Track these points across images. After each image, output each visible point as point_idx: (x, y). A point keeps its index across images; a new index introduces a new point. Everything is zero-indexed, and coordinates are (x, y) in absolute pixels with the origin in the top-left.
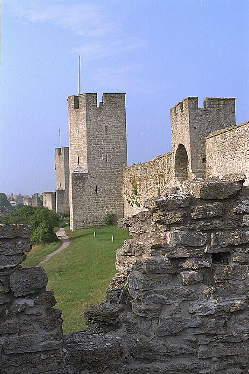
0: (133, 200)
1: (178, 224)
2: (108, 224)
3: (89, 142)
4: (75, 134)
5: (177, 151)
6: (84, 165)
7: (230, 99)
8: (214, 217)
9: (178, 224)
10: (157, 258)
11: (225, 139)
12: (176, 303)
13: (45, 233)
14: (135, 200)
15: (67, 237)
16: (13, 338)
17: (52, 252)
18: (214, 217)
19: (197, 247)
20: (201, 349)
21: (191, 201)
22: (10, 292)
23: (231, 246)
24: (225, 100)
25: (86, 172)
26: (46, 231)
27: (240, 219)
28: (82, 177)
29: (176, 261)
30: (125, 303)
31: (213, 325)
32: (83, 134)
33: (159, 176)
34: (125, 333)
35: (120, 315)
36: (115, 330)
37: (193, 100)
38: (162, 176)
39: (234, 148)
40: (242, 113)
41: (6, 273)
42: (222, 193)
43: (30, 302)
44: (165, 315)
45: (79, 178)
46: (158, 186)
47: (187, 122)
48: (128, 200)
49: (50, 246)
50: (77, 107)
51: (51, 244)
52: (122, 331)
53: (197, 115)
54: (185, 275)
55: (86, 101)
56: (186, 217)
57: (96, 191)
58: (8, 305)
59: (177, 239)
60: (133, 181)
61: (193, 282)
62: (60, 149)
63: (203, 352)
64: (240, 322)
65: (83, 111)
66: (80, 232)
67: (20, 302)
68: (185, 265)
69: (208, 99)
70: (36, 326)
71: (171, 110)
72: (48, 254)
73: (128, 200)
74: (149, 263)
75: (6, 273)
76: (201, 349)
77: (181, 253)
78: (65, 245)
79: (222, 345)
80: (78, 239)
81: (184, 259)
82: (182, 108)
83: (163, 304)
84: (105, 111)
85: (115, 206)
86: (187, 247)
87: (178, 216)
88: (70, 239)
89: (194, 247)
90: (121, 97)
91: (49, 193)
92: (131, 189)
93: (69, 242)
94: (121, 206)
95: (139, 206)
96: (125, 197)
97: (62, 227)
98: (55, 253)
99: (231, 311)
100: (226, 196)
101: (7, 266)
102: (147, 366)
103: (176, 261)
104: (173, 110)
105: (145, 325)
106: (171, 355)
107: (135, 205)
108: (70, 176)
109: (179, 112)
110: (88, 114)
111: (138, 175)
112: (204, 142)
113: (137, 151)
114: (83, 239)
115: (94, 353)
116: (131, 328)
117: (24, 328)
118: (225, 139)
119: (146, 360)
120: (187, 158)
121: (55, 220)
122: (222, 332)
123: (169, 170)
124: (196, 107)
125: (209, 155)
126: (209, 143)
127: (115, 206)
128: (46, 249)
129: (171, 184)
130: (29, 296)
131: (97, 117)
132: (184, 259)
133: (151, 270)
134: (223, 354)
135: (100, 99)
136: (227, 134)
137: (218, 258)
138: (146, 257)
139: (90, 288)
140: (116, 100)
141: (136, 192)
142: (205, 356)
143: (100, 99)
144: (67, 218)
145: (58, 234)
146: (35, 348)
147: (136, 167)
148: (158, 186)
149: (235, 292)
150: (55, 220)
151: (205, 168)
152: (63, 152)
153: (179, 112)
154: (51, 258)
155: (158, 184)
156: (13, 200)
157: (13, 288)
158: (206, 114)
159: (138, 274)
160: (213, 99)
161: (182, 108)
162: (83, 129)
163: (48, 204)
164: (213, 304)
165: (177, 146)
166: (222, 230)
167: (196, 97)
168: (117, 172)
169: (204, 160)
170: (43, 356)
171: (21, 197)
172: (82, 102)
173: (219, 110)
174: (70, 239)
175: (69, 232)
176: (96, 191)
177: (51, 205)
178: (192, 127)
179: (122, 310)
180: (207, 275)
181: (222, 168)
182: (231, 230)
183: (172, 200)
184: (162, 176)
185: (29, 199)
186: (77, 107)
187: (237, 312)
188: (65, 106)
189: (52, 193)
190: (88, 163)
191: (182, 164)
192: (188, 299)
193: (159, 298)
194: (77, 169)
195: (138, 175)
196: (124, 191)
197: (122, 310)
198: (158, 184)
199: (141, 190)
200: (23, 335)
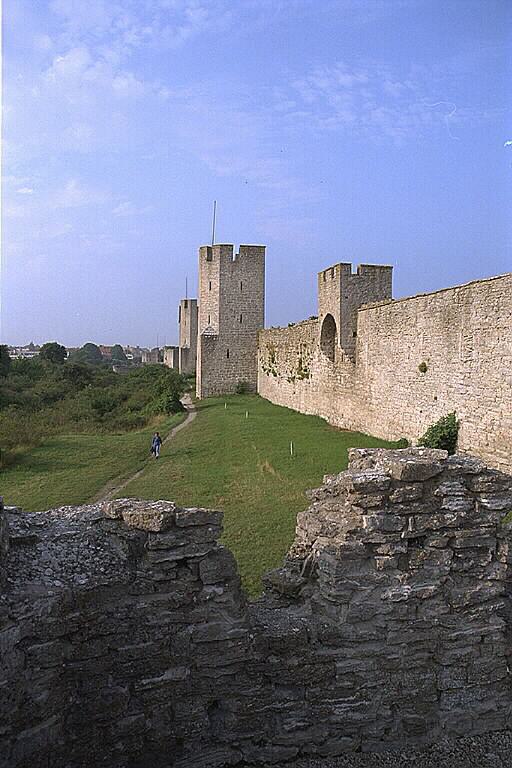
1: (376, 507)
5: (325, 321)
8: (413, 501)
9: (376, 507)
10: (352, 543)
12: (368, 589)
15: (193, 406)
16: (201, 627)
17: (178, 425)
18: (413, 501)
19: (394, 532)
20: (390, 635)
21: (392, 483)
22: (199, 580)
23: (429, 530)
25: (218, 333)
27: (441, 502)
29: (371, 547)
30: (307, 577)
31: (405, 611)
34: (310, 613)
35: (303, 589)
37: (346, 266)
39: (389, 324)
41: (196, 560)
42: (424, 474)
43: (220, 590)
44: (356, 601)
45: (209, 340)
46: (299, 356)
49: (175, 417)
50: (209, 259)
52: (306, 609)
53: (350, 283)
54: (380, 562)
56: (385, 500)
58: (196, 593)
59: (374, 524)
61: (387, 568)
63: (392, 639)
64: (432, 608)
65: (216, 264)
66: (208, 402)
67: (209, 590)
68: (379, 550)
70: (224, 613)
74: (344, 548)
75: (196, 560)
76: (390, 635)
77: (378, 538)
78: (192, 416)
79: (411, 631)
81: (379, 545)
83: (354, 590)
84: (242, 265)
86: (385, 532)
87: (377, 499)
88: (197, 409)
89: (390, 532)
90: (386, 270)
91: (170, 348)
97: (187, 392)
98: (181, 426)
99: (424, 597)
100: (427, 477)
101: (197, 555)
102: (335, 652)
103: (371, 547)
105: (334, 610)
106: (360, 641)
108: (199, 337)
109: (329, 278)
111: (277, 340)
112: (357, 314)
113: (277, 312)
114: (212, 410)
115: (282, 640)
116: (316, 608)
117: (211, 615)
119: (336, 646)
120: (335, 329)
121: (180, 383)
122: (413, 617)
124: (349, 275)
126: (361, 315)
128: (171, 421)
130: (219, 584)
132: (379, 545)
133: (347, 554)
134: (413, 640)
135: (236, 251)
136: (383, 308)
137: (416, 542)
138: (340, 541)
139: (226, 477)
140: (254, 254)
141: (273, 359)
142: (394, 643)
143: (236, 251)
144: (192, 380)
145: (183, 401)
146: (221, 637)
147: (275, 330)
148: (299, 356)
149: (430, 577)
150: (180, 383)
152: (191, 306)
153: (329, 278)
156: (130, 353)
157: (202, 577)
159: (329, 558)
163: (169, 361)
164: (406, 590)
165: (325, 316)
166: (421, 514)
169: (355, 334)
170: (231, 644)
172: (216, 254)
174: (197, 409)
175: (195, 400)
179: (305, 583)
180: (402, 562)
182: (430, 514)
183: (370, 482)
184: (305, 345)
185: (149, 355)
186: (209, 259)
187: (430, 598)
188: (197, 258)
189: (173, 348)
191: (328, 336)
192: (382, 585)
193: (351, 584)
195: (277, 340)
196: (258, 357)
197: (305, 583)
200: (210, 624)
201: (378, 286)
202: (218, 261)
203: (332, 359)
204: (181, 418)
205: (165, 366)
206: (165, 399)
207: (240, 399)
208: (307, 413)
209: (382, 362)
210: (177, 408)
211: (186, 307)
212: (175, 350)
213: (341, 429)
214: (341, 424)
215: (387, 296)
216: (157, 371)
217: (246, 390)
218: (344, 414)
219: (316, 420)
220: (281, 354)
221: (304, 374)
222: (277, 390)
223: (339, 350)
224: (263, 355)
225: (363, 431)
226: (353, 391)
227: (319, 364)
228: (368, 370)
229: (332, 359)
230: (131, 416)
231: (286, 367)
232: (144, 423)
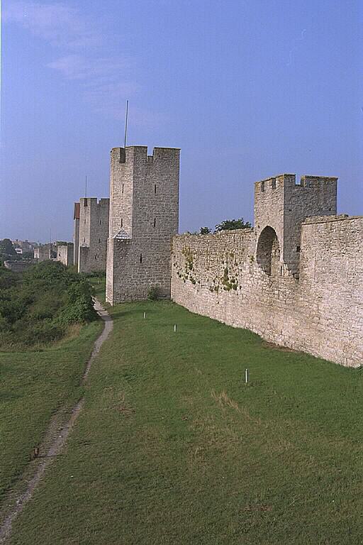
0: (186, 275)
2: (153, 299)
3: (135, 203)
4: (121, 193)
6: (128, 229)
7: (332, 179)
11: (331, 229)
13: (85, 310)
14: (189, 276)
24: (326, 179)
25: (131, 237)
26: (86, 308)
28: (125, 242)
32: (129, 193)
33: (227, 254)
36: (60, 339)
37: (290, 177)
38: (232, 255)
40: (343, 202)
47: (281, 202)
48: (178, 273)
50: (123, 161)
51: (93, 324)
55: (135, 155)
57: (141, 260)
60: (188, 253)
62: (86, 199)
65: (130, 167)
66: (122, 308)
69: (307, 177)
71: (256, 184)
72: (95, 340)
73: (178, 273)
78: (109, 325)
80: (123, 317)
82: (274, 184)
85: (161, 279)
88: (112, 317)
90: (174, 153)
92: (184, 262)
93: (112, 322)
94: (169, 279)
95: (195, 283)
96: (174, 270)
104: (260, 185)
107: (188, 281)
109: (268, 187)
110: (136, 170)
112: (300, 228)
114: (130, 318)
118: (331, 229)
123: (243, 250)
125: (305, 245)
126: (307, 230)
127: (161, 279)
129: (245, 268)
131: (146, 175)
135: (150, 153)
140: (168, 156)
150: (90, 284)
151: (299, 258)
152: (101, 208)
153: (268, 187)
154: (103, 346)
155: (225, 264)
156: (19, 247)
158: (303, 195)
160: (313, 177)
161: (274, 184)
162: (129, 186)
163: (63, 257)
167: (293, 174)
168: (165, 239)
169: (299, 249)
171: (26, 243)
172: (130, 155)
173: (319, 191)
176: (141, 260)
177: (66, 259)
178: (287, 210)
181: (325, 263)
184: (232, 255)
185: (42, 249)
186: (123, 161)
190: (133, 227)
194: (119, 233)
198: (225, 264)
199: (199, 266)
201: (322, 198)
202: (132, 164)
203: (268, 272)
204: (98, 328)
205: (59, 263)
206: (80, 307)
207: (153, 306)
208: (235, 326)
209: (335, 281)
210: (92, 316)
211: (86, 205)
212: (70, 246)
213: (282, 347)
214: (280, 342)
215: (332, 210)
216: (58, 271)
217: (159, 296)
218: (284, 331)
219: (246, 336)
220: (199, 263)
221: (232, 286)
222: (198, 296)
223: (279, 262)
224: (178, 262)
225: (308, 350)
226: (294, 308)
227: (250, 276)
228: (315, 288)
229: (268, 272)
230: (46, 325)
231: (207, 276)
232: (58, 334)
